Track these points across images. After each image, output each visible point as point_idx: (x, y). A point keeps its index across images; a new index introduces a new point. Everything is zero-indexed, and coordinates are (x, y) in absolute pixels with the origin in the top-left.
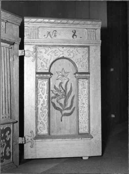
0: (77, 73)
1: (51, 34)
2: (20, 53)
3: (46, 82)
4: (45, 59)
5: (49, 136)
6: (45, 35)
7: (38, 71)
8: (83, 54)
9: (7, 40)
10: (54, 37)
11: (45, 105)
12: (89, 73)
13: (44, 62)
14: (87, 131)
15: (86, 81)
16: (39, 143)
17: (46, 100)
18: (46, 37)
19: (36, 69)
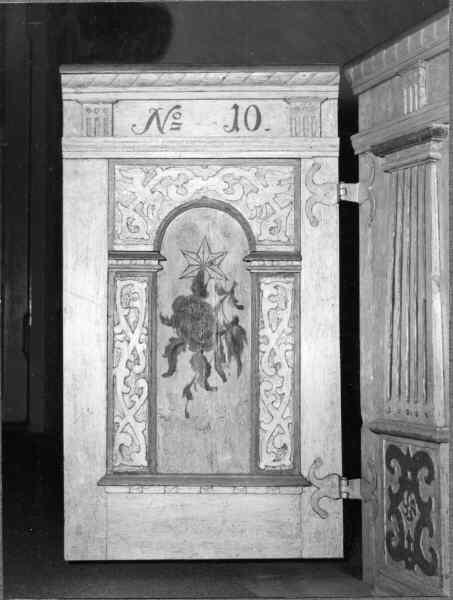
0: (254, 255)
1: (162, 119)
2: (354, 193)
3: (140, 287)
4: (268, 203)
5: (151, 475)
6: (134, 125)
7: (116, 248)
8: (278, 190)
9: (417, 147)
10: (172, 129)
11: (138, 369)
12: (298, 256)
13: (136, 216)
14: (287, 462)
15: (286, 284)
16: (119, 497)
17: (141, 348)
18: (228, 129)
19: (112, 236)
